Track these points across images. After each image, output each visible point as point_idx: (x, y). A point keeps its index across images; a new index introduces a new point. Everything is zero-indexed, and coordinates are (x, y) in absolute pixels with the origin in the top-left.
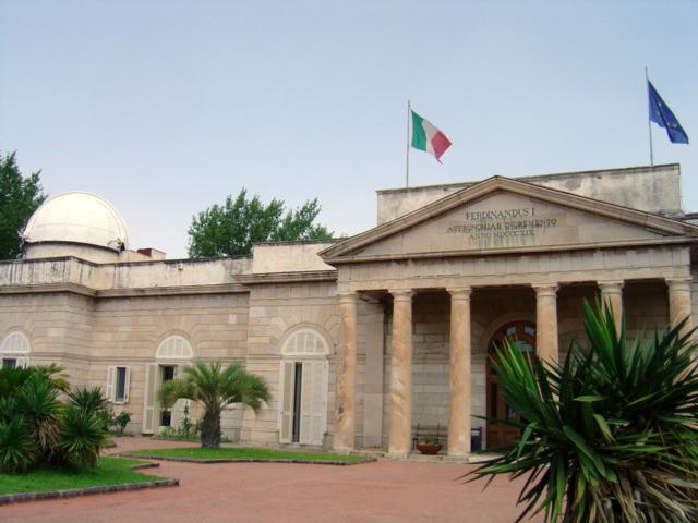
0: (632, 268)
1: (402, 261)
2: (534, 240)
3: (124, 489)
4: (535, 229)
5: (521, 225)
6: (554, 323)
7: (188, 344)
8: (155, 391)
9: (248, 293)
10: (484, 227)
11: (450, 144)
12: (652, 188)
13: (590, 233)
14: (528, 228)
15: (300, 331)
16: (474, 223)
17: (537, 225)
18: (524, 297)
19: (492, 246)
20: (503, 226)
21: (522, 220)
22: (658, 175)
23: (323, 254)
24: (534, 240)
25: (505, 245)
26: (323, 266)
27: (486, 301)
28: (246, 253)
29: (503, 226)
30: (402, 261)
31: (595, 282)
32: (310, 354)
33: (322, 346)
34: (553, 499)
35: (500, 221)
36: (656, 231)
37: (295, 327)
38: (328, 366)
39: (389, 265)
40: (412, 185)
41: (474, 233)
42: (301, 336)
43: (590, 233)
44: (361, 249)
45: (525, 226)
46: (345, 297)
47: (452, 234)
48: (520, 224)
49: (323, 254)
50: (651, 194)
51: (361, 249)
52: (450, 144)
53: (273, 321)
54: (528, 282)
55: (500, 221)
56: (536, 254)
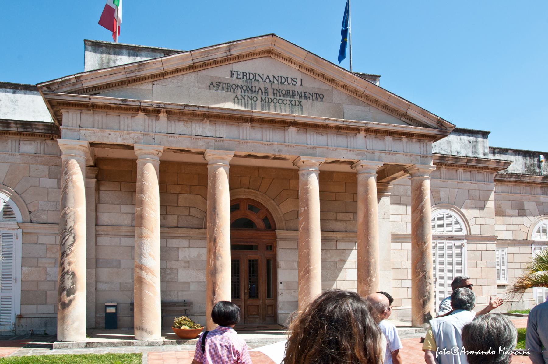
0: (97, 98)
1: (154, 112)
2: (302, 111)
5: (290, 94)
10: (249, 89)
11: (100, 23)
14: (296, 98)
16: (240, 82)
17: (306, 97)
18: (288, 180)
20: (270, 92)
21: (291, 88)
24: (302, 111)
25: (272, 111)
29: (270, 92)
30: (154, 112)
33: (12, 213)
35: (268, 84)
38: (20, 235)
39: (134, 116)
41: (238, 92)
44: (96, 90)
45: (293, 96)
47: (213, 91)
48: (288, 93)
51: (96, 90)
52: (100, 23)
55: (268, 84)
56: (305, 126)
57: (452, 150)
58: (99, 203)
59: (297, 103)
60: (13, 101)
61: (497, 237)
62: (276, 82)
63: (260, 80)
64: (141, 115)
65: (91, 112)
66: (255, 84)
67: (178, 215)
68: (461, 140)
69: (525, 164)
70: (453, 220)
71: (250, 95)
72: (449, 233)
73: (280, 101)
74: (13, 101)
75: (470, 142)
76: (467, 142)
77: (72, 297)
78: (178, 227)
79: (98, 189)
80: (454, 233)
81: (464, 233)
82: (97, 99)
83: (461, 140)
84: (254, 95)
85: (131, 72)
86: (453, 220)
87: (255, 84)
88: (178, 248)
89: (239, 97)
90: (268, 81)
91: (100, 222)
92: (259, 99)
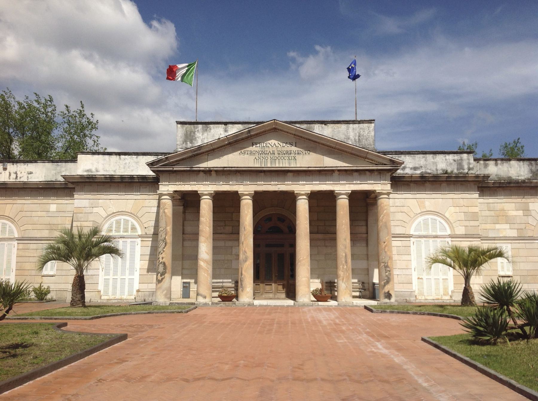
3: (131, 314)
4: (297, 156)
6: (307, 215)
7: (13, 226)
8: (424, 256)
9: (74, 188)
12: (358, 134)
13: (329, 162)
14: (292, 155)
15: (427, 217)
17: (298, 154)
19: (269, 165)
20: (276, 153)
22: (361, 125)
23: (151, 165)
25: (277, 165)
26: (148, 172)
27: (219, 198)
28: (74, 160)
29: (276, 153)
31: (196, 192)
32: (125, 234)
34: (488, 303)
36: (373, 162)
37: (114, 214)
40: (359, 119)
41: (257, 156)
42: (118, 222)
43: (329, 162)
46: (247, 195)
49: (151, 165)
50: (357, 138)
51: (177, 163)
53: (95, 210)
54: (236, 190)
55: (274, 149)
57: (438, 168)
58: (185, 220)
59: (293, 158)
60: (136, 163)
61: (48, 292)
62: (279, 146)
63: (270, 146)
64: (202, 173)
65: (175, 174)
66: (267, 149)
67: (233, 226)
68: (446, 160)
69: (531, 170)
70: (438, 223)
71: (263, 156)
72: (434, 234)
73: (282, 158)
74: (136, 163)
75: (454, 161)
76: (452, 161)
77: (163, 276)
78: (232, 234)
79: (184, 212)
80: (439, 233)
81: (449, 232)
82: (176, 168)
83: (446, 160)
84: (266, 156)
85: (195, 151)
86: (438, 223)
87: (267, 149)
88: (232, 247)
89: (257, 158)
90: (274, 146)
91: (186, 232)
92: (269, 158)
